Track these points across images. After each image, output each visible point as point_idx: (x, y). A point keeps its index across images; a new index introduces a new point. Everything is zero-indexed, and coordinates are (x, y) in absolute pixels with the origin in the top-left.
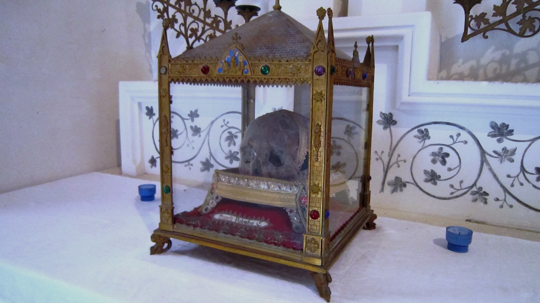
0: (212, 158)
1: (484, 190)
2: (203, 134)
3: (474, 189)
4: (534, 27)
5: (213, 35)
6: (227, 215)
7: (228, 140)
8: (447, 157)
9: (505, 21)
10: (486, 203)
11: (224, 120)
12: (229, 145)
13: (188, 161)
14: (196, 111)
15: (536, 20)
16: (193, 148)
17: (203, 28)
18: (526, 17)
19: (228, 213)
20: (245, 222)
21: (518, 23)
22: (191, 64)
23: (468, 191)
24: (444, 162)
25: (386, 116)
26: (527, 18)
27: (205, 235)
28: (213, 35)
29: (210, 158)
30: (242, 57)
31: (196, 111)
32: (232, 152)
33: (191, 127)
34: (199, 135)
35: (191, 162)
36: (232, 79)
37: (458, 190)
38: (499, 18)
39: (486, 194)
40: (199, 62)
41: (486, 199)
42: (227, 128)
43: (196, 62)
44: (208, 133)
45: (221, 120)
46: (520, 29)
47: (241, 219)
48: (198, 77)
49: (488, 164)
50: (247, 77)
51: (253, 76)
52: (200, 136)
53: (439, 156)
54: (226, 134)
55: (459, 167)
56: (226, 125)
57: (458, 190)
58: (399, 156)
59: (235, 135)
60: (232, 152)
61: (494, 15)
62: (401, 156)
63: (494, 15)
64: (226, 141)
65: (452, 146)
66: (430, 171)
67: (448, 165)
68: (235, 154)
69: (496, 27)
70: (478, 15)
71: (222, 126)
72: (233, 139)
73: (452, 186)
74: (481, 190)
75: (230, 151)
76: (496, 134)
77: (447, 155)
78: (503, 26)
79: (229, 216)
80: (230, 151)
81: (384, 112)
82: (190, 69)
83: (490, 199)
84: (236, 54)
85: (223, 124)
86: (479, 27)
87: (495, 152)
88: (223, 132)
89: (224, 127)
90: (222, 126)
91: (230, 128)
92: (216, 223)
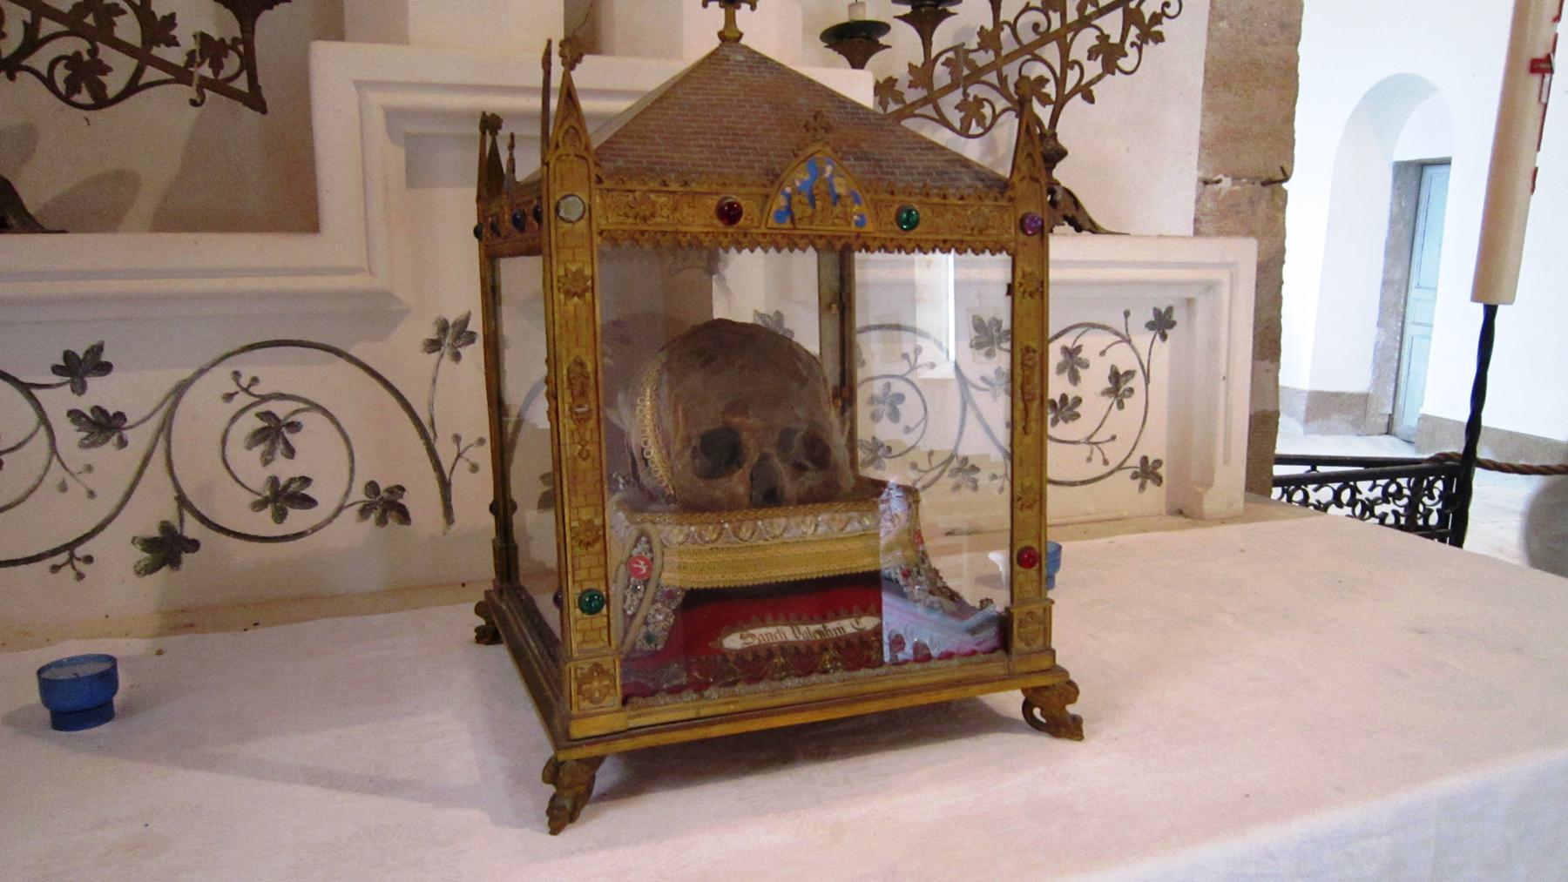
0: (188, 517)
1: (971, 462)
2: (138, 439)
3: (955, 464)
4: (983, 117)
5: (86, 57)
6: (763, 630)
7: (256, 445)
8: (900, 403)
9: (931, 99)
10: (975, 488)
11: (236, 374)
12: (267, 460)
13: (70, 547)
14: (97, 349)
15: (986, 103)
16: (91, 494)
17: (31, 29)
18: (968, 95)
19: (763, 623)
20: (818, 632)
21: (956, 107)
22: (674, 193)
23: (943, 471)
24: (895, 416)
25: (768, 320)
26: (971, 99)
27: (737, 702)
28: (86, 57)
29: (182, 521)
30: (843, 181)
31: (97, 349)
32: (282, 481)
33: (75, 415)
34: (115, 439)
35: (80, 551)
36: (834, 242)
37: (926, 472)
38: (920, 93)
39: (975, 469)
40: (705, 188)
41: (975, 481)
42: (252, 400)
43: (694, 187)
44: (166, 427)
45: (224, 372)
46: (962, 121)
47: (803, 628)
48: (707, 234)
49: (974, 407)
50: (862, 235)
51: (878, 234)
52: (123, 443)
53: (884, 403)
54: (251, 423)
55: (923, 423)
56: (246, 390)
57: (926, 472)
58: (457, 438)
59: (290, 420)
60: (282, 481)
61: (912, 85)
62: (463, 437)
63: (912, 85)
64: (249, 448)
65: (907, 377)
66: (870, 441)
67: (904, 421)
68: (294, 487)
69: (917, 112)
70: (881, 81)
71: (229, 397)
72: (278, 433)
73: (914, 466)
74: (967, 462)
75: (274, 481)
76: (982, 340)
77: (900, 398)
78: (929, 110)
79: (772, 630)
80: (274, 481)
81: (762, 311)
82: (675, 209)
83: (982, 478)
84: (824, 171)
85: (233, 388)
86: (885, 110)
87: (983, 379)
88: (234, 419)
89: (236, 397)
90: (229, 397)
91: (264, 399)
92: (750, 658)
